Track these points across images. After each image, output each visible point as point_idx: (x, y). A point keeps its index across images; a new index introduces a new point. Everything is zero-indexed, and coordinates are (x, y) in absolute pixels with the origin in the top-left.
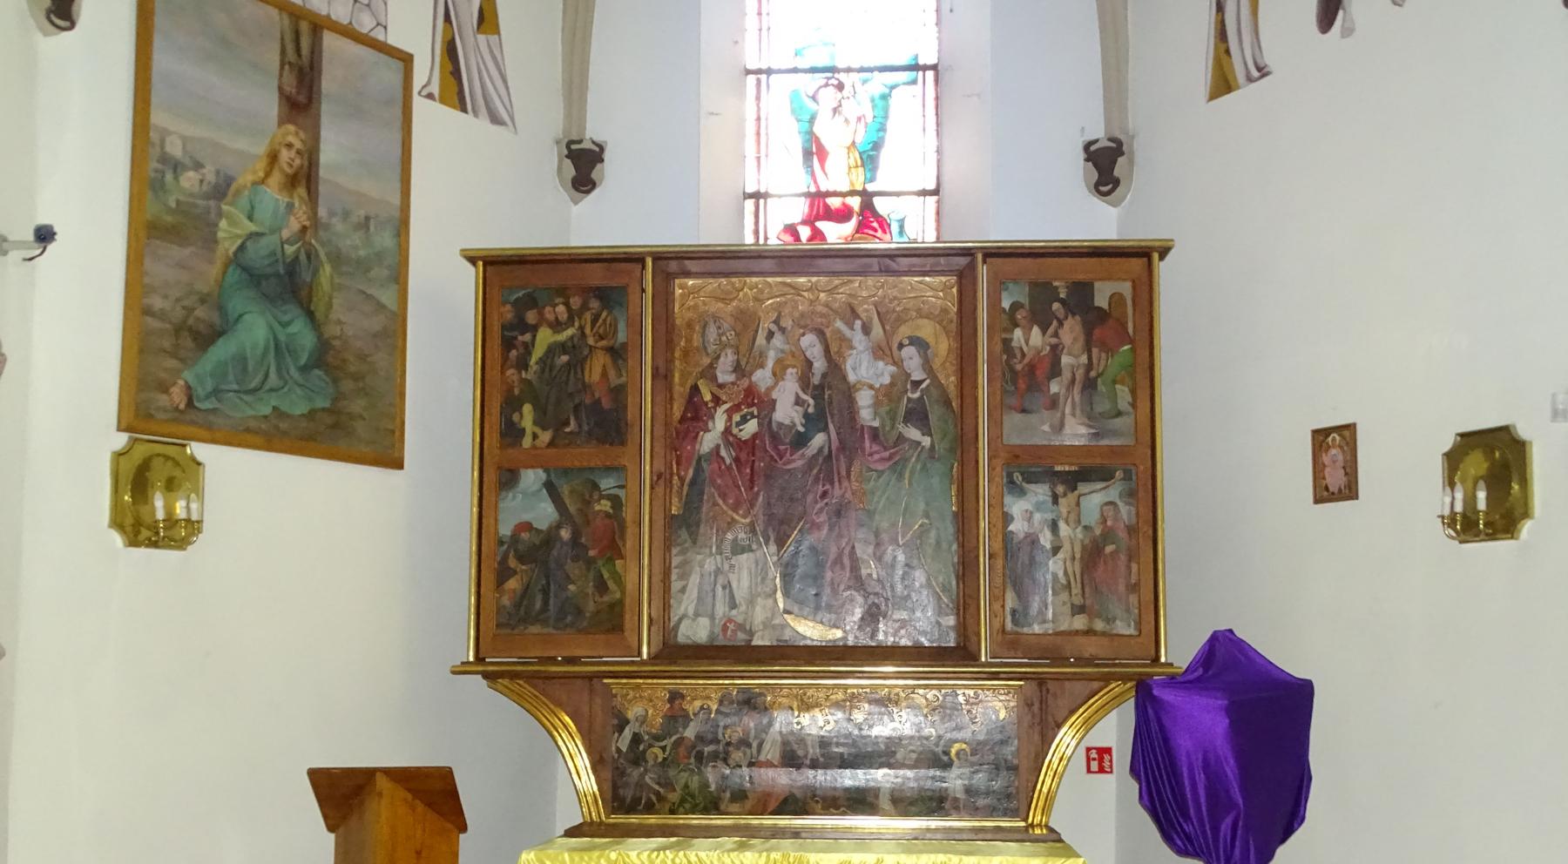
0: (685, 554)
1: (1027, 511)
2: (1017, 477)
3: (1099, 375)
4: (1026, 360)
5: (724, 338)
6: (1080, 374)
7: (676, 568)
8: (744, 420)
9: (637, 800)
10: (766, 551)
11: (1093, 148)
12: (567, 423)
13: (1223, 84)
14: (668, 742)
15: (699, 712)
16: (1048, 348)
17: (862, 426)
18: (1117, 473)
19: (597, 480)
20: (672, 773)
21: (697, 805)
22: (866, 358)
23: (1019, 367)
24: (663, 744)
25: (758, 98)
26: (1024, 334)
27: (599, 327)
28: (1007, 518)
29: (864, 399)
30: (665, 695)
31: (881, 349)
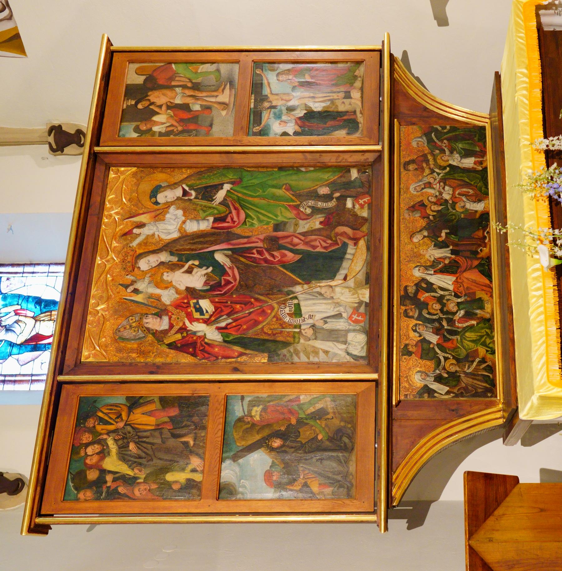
0: (298, 351)
1: (280, 124)
2: (257, 129)
3: (190, 81)
4: (175, 123)
5: (134, 325)
7: (309, 358)
8: (200, 310)
9: (486, 379)
10: (299, 293)
11: (55, 147)
12: (186, 444)
14: (441, 355)
15: (418, 332)
16: (169, 111)
17: (212, 228)
18: (258, 72)
19: (235, 419)
20: (463, 353)
21: (487, 334)
22: (161, 226)
23: (180, 128)
24: (442, 359)
26: (156, 125)
27: (111, 418)
29: (192, 227)
30: (405, 359)
31: (156, 216)
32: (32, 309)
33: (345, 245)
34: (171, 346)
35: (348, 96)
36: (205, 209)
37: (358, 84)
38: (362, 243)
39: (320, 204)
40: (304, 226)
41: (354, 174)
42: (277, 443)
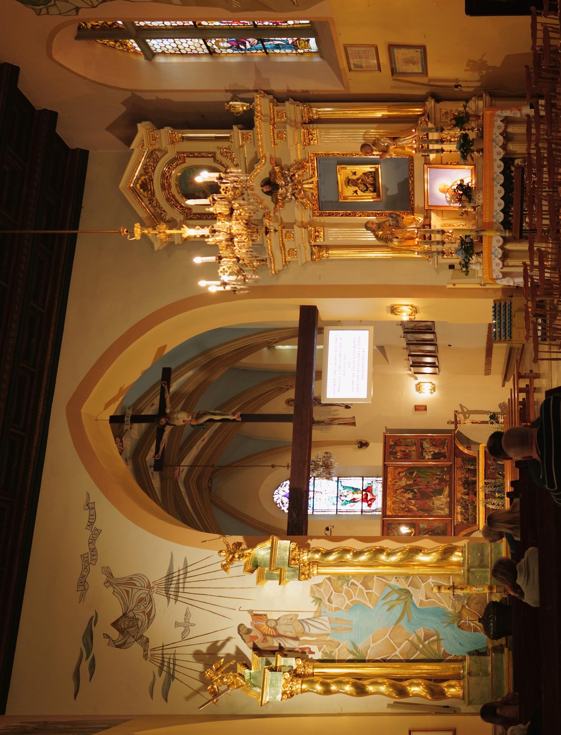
6: (405, 447)
8: (412, 503)
9: (475, 520)
13: (354, 424)
14: (465, 514)
22: (401, 482)
25: (342, 512)
28: (429, 459)
29: (408, 483)
32: (352, 491)
33: (444, 487)
34: (406, 511)
35: (444, 448)
36: (411, 478)
37: (446, 445)
38: (447, 487)
39: (438, 477)
40: (434, 482)
41: (445, 469)
42: (430, 533)
